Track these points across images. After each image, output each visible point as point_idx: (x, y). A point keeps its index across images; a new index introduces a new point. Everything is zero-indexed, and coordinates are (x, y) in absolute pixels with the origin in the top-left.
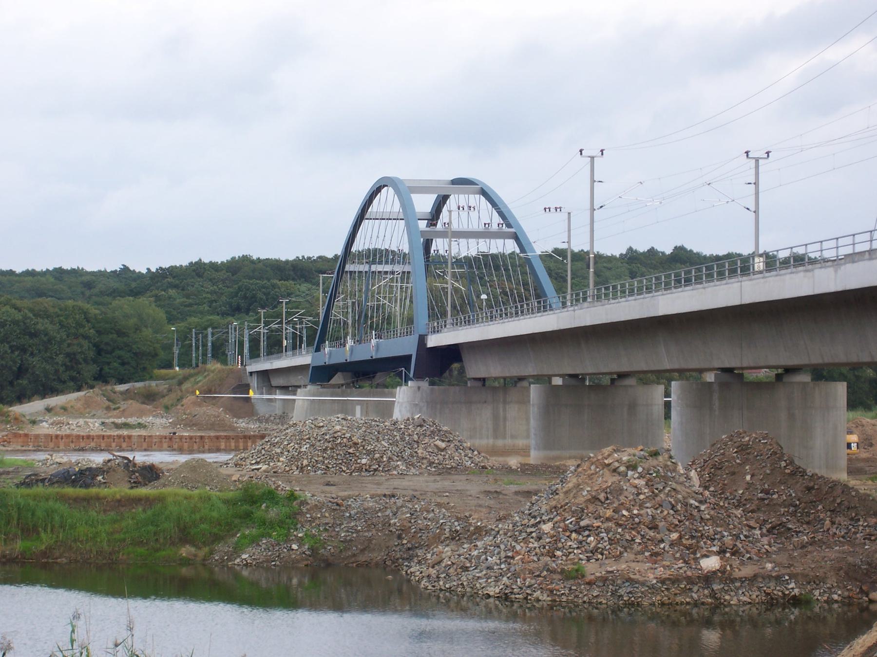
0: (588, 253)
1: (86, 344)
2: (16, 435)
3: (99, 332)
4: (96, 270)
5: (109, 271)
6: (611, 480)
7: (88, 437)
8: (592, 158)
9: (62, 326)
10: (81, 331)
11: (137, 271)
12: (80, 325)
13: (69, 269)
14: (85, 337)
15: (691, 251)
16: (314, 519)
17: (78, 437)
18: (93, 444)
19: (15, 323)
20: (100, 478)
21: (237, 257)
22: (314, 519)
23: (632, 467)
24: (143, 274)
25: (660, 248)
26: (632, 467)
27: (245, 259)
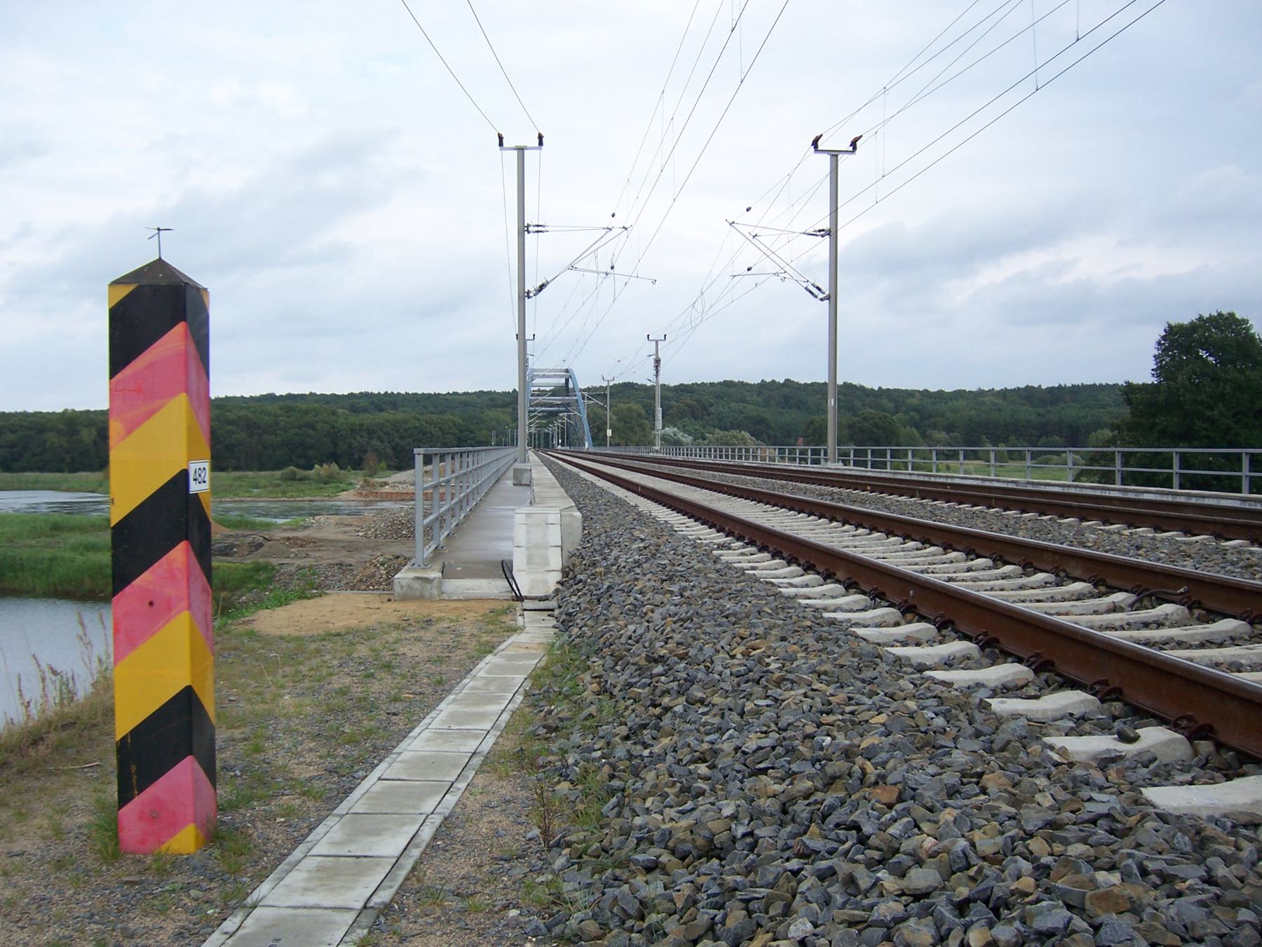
0: (818, 390)
1: (452, 437)
2: (372, 493)
3: (460, 431)
4: (904, 389)
5: (1044, 387)
6: (373, 570)
7: (407, 493)
8: (521, 150)
9: (440, 428)
10: (451, 431)
11: (395, 393)
12: (450, 428)
13: (876, 388)
14: (454, 434)
15: (1138, 384)
16: (280, 580)
17: (402, 493)
18: (408, 497)
19: (416, 428)
20: (235, 550)
21: (1156, 352)
22: (280, 580)
23: (383, 564)
24: (1144, 388)
25: (401, 392)
26: (383, 564)
27: (682, 385)
